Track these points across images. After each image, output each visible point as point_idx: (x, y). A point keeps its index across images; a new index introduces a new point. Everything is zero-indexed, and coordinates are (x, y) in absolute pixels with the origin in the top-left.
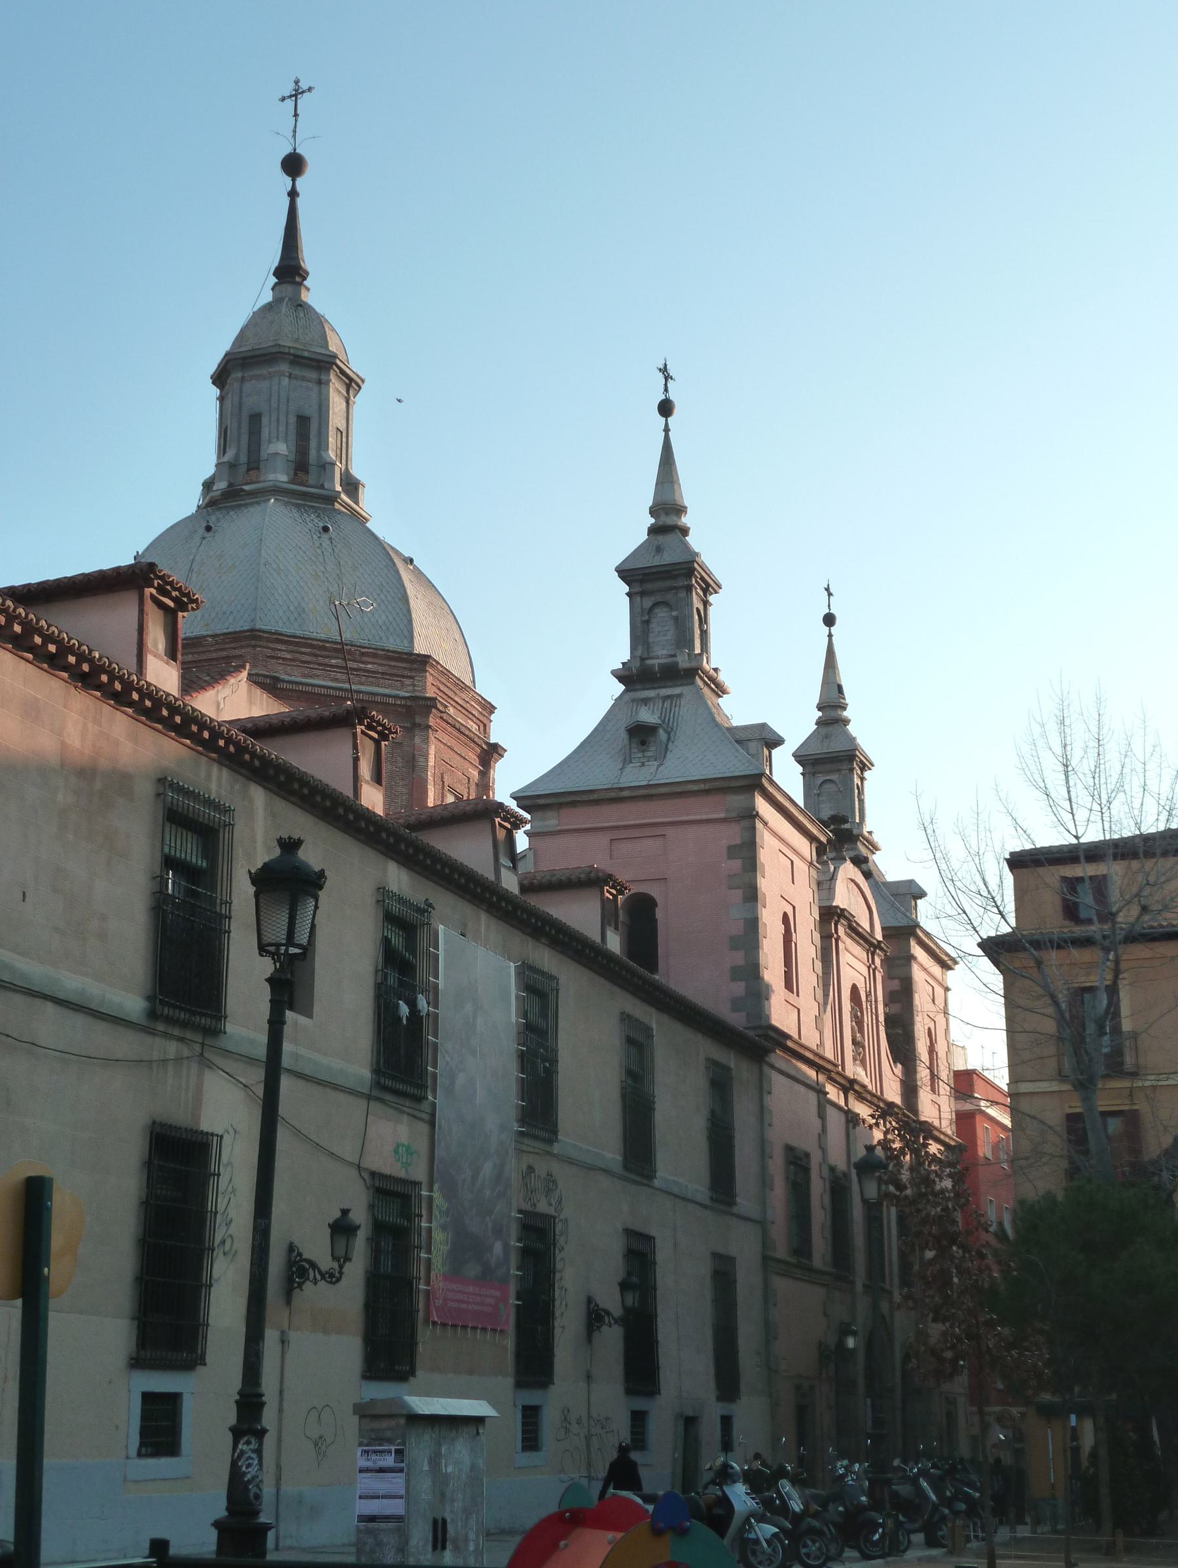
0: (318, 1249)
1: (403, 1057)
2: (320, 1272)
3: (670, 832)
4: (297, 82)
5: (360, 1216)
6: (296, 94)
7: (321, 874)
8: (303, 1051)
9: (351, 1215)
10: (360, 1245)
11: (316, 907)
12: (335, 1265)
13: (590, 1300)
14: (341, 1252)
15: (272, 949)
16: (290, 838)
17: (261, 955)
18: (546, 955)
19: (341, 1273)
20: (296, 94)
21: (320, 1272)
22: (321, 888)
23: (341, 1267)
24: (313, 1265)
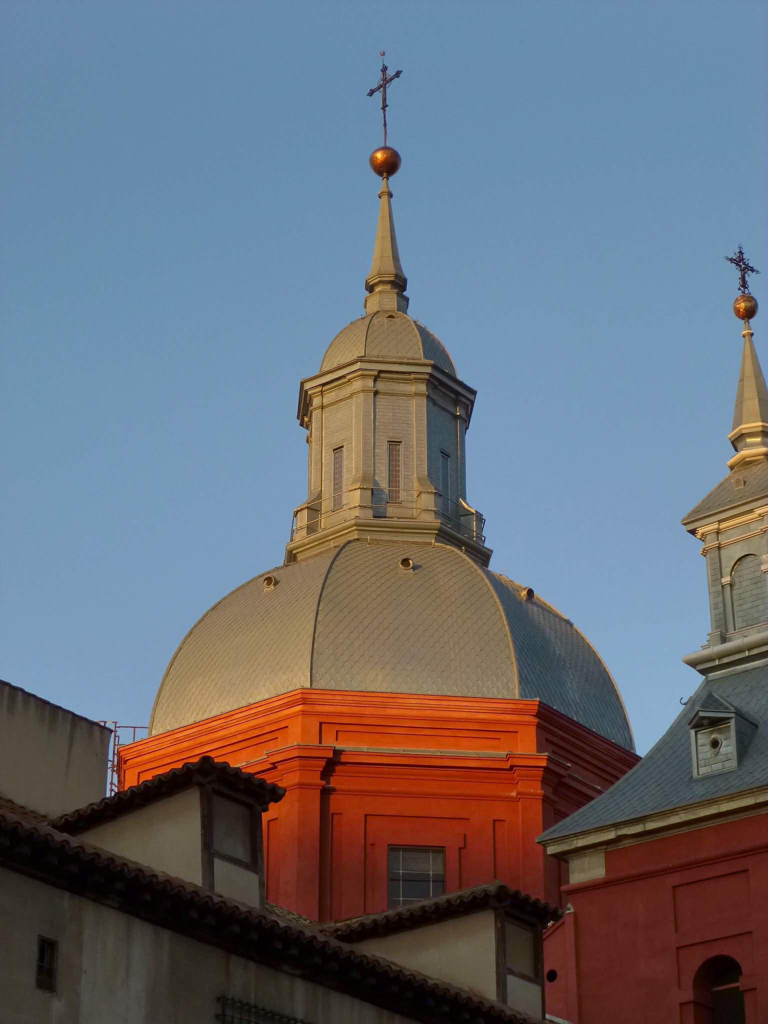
4: (384, 69)
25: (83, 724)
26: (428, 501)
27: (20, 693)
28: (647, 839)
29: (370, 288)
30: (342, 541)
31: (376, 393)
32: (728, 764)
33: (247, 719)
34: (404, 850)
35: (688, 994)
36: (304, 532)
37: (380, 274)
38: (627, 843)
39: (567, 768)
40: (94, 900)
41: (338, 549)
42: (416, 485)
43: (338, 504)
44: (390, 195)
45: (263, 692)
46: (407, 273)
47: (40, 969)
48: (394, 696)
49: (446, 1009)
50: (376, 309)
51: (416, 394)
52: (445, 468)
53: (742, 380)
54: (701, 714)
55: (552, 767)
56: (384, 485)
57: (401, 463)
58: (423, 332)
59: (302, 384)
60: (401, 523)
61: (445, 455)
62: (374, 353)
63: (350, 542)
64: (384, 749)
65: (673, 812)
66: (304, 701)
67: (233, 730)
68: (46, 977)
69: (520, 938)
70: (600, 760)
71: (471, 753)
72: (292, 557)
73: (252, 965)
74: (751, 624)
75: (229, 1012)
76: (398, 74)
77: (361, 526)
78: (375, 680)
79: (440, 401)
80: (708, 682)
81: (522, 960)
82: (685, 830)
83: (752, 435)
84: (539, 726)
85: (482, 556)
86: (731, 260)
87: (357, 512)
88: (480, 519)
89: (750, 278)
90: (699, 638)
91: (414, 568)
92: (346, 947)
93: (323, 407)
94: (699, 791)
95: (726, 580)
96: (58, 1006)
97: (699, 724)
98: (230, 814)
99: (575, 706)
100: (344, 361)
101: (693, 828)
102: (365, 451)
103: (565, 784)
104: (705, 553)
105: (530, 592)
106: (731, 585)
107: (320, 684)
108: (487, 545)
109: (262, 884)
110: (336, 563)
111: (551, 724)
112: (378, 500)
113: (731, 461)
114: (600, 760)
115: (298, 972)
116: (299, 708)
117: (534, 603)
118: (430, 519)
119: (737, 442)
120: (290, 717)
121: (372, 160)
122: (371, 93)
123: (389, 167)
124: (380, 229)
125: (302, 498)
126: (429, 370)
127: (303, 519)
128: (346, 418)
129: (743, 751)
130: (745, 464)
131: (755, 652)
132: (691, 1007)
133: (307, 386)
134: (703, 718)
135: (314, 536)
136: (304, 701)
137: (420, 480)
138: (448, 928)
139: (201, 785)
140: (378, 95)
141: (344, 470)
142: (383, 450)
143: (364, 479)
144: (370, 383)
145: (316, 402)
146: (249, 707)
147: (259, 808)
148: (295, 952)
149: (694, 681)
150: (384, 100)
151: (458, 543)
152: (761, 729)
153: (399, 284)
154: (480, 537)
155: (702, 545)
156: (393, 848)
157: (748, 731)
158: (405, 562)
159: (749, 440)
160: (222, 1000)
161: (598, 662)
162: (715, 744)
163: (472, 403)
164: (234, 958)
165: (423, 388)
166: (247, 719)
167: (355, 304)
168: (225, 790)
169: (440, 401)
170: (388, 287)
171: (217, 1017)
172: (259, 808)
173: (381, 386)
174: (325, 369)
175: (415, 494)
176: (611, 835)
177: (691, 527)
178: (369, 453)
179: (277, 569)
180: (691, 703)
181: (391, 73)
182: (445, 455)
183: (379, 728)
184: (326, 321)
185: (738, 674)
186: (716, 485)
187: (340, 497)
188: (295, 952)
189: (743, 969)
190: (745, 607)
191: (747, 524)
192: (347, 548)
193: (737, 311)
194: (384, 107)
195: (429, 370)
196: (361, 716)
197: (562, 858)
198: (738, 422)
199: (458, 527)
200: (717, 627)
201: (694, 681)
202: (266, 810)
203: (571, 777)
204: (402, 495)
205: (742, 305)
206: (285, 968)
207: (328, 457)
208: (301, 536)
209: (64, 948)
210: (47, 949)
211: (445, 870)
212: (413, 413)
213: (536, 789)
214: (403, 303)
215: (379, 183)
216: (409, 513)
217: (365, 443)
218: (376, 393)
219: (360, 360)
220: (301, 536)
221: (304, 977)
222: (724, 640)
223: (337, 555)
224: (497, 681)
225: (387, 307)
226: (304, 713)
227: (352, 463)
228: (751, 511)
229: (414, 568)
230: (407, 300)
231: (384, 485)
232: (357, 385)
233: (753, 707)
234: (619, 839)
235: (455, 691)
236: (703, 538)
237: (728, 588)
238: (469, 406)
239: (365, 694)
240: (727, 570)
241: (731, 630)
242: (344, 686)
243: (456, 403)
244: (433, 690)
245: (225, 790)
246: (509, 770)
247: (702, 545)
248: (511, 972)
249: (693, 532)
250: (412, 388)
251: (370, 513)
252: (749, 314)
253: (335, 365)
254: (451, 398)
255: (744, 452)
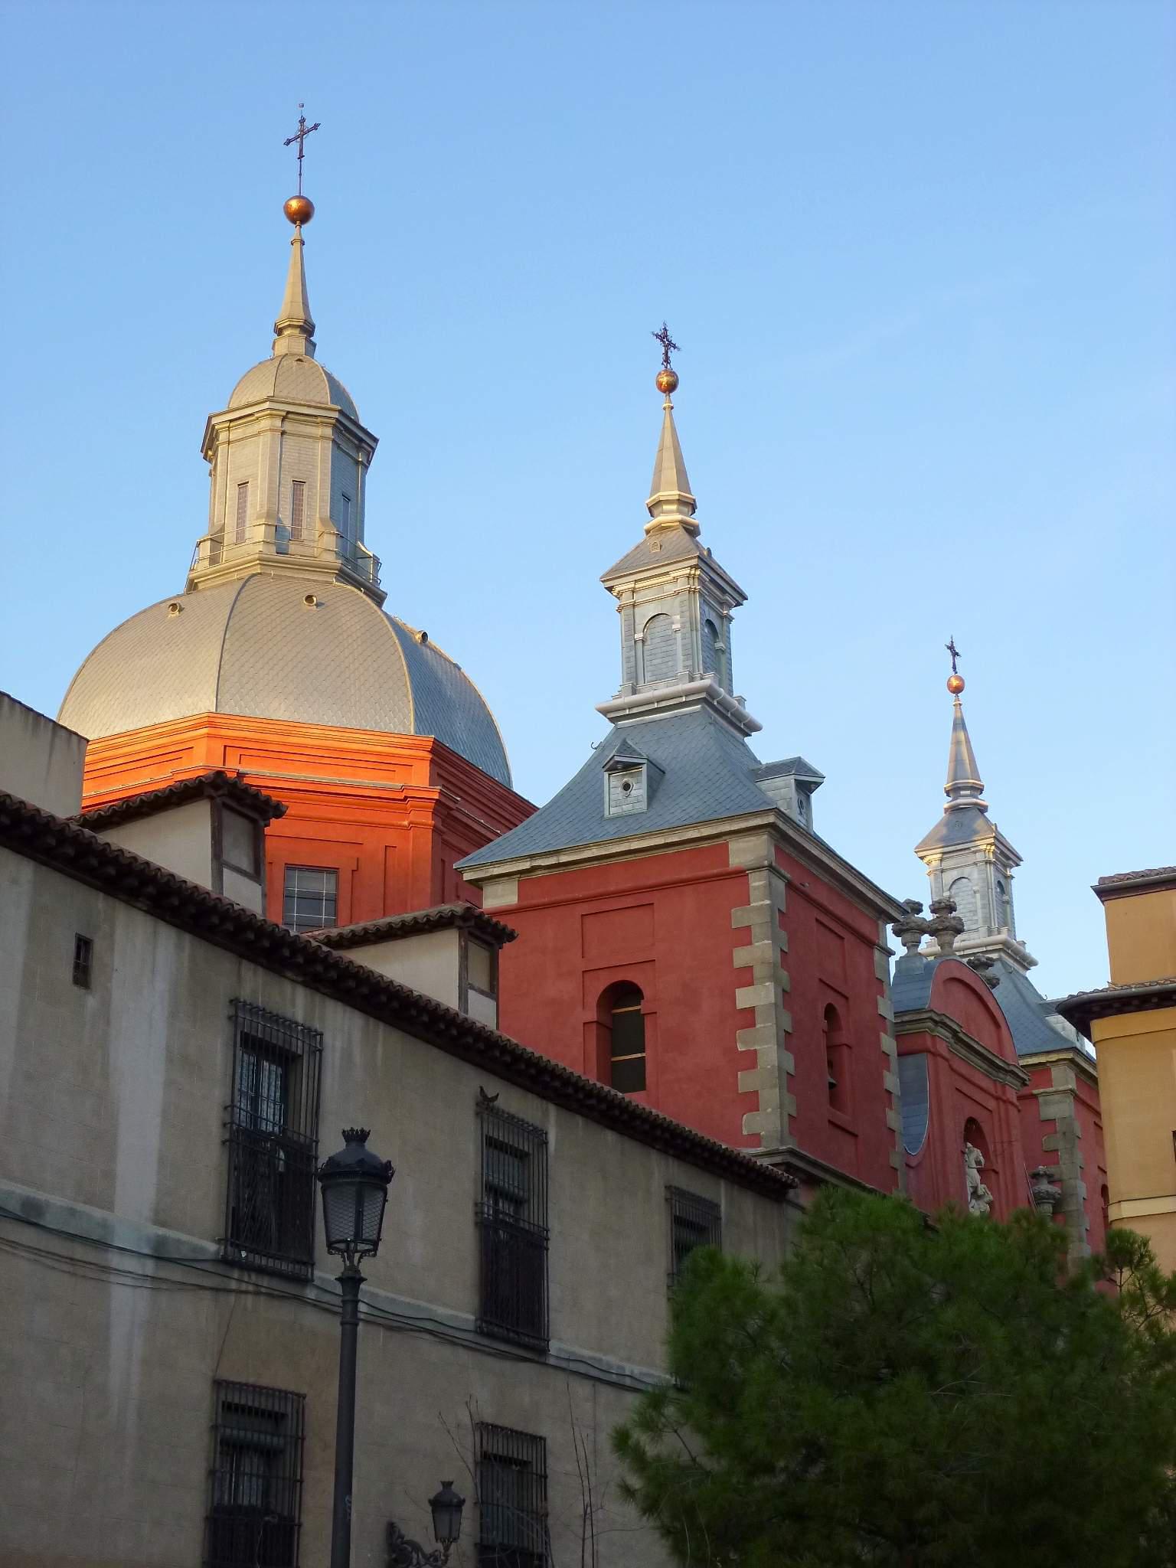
0: (419, 1528)
1: (512, 1299)
2: (424, 1555)
3: (655, 897)
4: (302, 121)
5: (466, 1488)
6: (303, 133)
7: (388, 1166)
8: (563, 1346)
9: (370, 1146)
10: (468, 1522)
11: (385, 1200)
12: (440, 1546)
13: (391, 1528)
14: (445, 1532)
15: (342, 1246)
16: (352, 1130)
17: (330, 1253)
18: (255, 1460)
19: (447, 1556)
20: (303, 133)
21: (424, 1555)
22: (389, 1180)
23: (447, 1549)
24: (417, 1548)
25: (63, 733)
26: (330, 541)
27: (6, 699)
28: (561, 870)
29: (279, 331)
30: (246, 574)
31: (283, 433)
32: (637, 806)
33: (150, 738)
34: (300, 870)
35: (592, 1015)
36: (206, 563)
37: (290, 318)
38: (540, 873)
39: (456, 802)
40: (127, 902)
41: (241, 583)
42: (318, 525)
43: (240, 538)
44: (303, 243)
45: (168, 713)
46: (315, 320)
47: (77, 966)
48: (297, 725)
49: (425, 1018)
50: (284, 351)
51: (322, 437)
52: (346, 508)
53: (661, 450)
54: (617, 759)
55: (443, 800)
56: (287, 523)
57: (305, 503)
58: (328, 375)
59: (210, 419)
60: (303, 560)
61: (347, 498)
62: (283, 394)
63: (254, 575)
64: (295, 775)
65: (586, 846)
66: (211, 724)
67: (137, 747)
68: (82, 975)
69: (479, 956)
70: (484, 796)
71: (367, 782)
72: (192, 586)
73: (260, 971)
74: (659, 677)
75: (240, 1014)
76: (316, 127)
77: (263, 561)
78: (279, 710)
79: (344, 446)
80: (617, 729)
81: (479, 976)
82: (596, 864)
83: (668, 502)
84: (432, 761)
85: (379, 598)
86: (657, 336)
87: (260, 547)
88: (377, 562)
89: (673, 354)
90: (611, 688)
91: (317, 605)
92: (336, 953)
93: (229, 442)
94: (611, 829)
95: (639, 636)
96: (92, 1002)
97: (613, 768)
98: (237, 828)
99: (465, 747)
100: (252, 400)
101: (604, 862)
102: (270, 488)
103: (456, 819)
104: (619, 610)
105: (425, 636)
106: (643, 641)
107: (226, 709)
108: (382, 587)
109: (264, 895)
110: (242, 594)
111: (442, 758)
112: (281, 536)
113: (647, 526)
114: (484, 796)
115: (300, 979)
116: (205, 731)
117: (428, 647)
118: (332, 559)
119: (652, 509)
120: (194, 739)
121: (287, 207)
122: (288, 142)
123: (302, 216)
124: (291, 277)
125: (204, 532)
126: (336, 415)
127: (206, 549)
128: (252, 455)
129: (652, 795)
130: (661, 529)
131: (663, 704)
132: (594, 1026)
133: (214, 421)
134: (618, 762)
135: (217, 567)
136: (211, 724)
137: (321, 519)
138: (414, 942)
139: (211, 798)
140: (295, 145)
141: (248, 504)
142: (287, 490)
143: (268, 515)
144: (278, 423)
145: (223, 437)
146: (154, 727)
147: (262, 823)
148: (300, 960)
149: (604, 728)
150: (301, 150)
151: (358, 585)
152: (667, 776)
153: (308, 329)
154: (376, 580)
155: (617, 603)
156: (290, 867)
157: (657, 776)
158: (309, 598)
159: (666, 507)
160: (234, 1002)
161: (483, 705)
162: (626, 787)
163: (374, 449)
164: (245, 962)
165: (329, 431)
166: (150, 738)
167: (262, 346)
168: (234, 804)
169: (344, 446)
170: (297, 331)
171: (230, 1018)
172: (262, 823)
173: (288, 426)
174: (233, 405)
175: (317, 534)
176: (526, 865)
177: (609, 584)
178: (274, 493)
179: (179, 596)
180: (602, 748)
181: (309, 124)
182: (347, 498)
183: (283, 755)
184: (235, 360)
185: (646, 724)
186: (632, 547)
187: (243, 531)
188: (300, 960)
189: (645, 994)
190: (655, 662)
191: (661, 584)
192: (252, 581)
193: (659, 385)
194: (301, 157)
195: (336, 415)
196: (264, 742)
197: (478, 884)
198: (656, 489)
199: (355, 568)
200: (629, 679)
201: (604, 728)
202: (267, 825)
203: (458, 810)
204: (305, 534)
205: (665, 380)
206: (289, 974)
207: (233, 491)
208: (203, 567)
209: (98, 946)
210: (83, 945)
211: (337, 889)
212: (318, 454)
213: (428, 819)
214: (311, 346)
215: (292, 230)
216: (308, 551)
217: (271, 482)
218: (283, 433)
219: (268, 399)
220: (203, 567)
221: (305, 984)
222: (634, 692)
223: (244, 586)
224: (394, 719)
225: (295, 351)
226: (209, 736)
227: (257, 499)
228: (667, 573)
229: (317, 605)
230: (314, 345)
231: (287, 523)
232: (265, 423)
233: (661, 756)
234: (533, 869)
235: (354, 724)
236: (619, 596)
237: (640, 644)
238: (370, 452)
239: (269, 721)
240: (640, 627)
241: (641, 683)
242: (247, 712)
243: (359, 448)
244: (334, 722)
245: (234, 804)
246: (403, 800)
247: (617, 603)
248: (472, 988)
249: (610, 589)
250: (319, 431)
251: (273, 549)
252: (671, 388)
253: (243, 403)
254: (354, 442)
255: (661, 519)
